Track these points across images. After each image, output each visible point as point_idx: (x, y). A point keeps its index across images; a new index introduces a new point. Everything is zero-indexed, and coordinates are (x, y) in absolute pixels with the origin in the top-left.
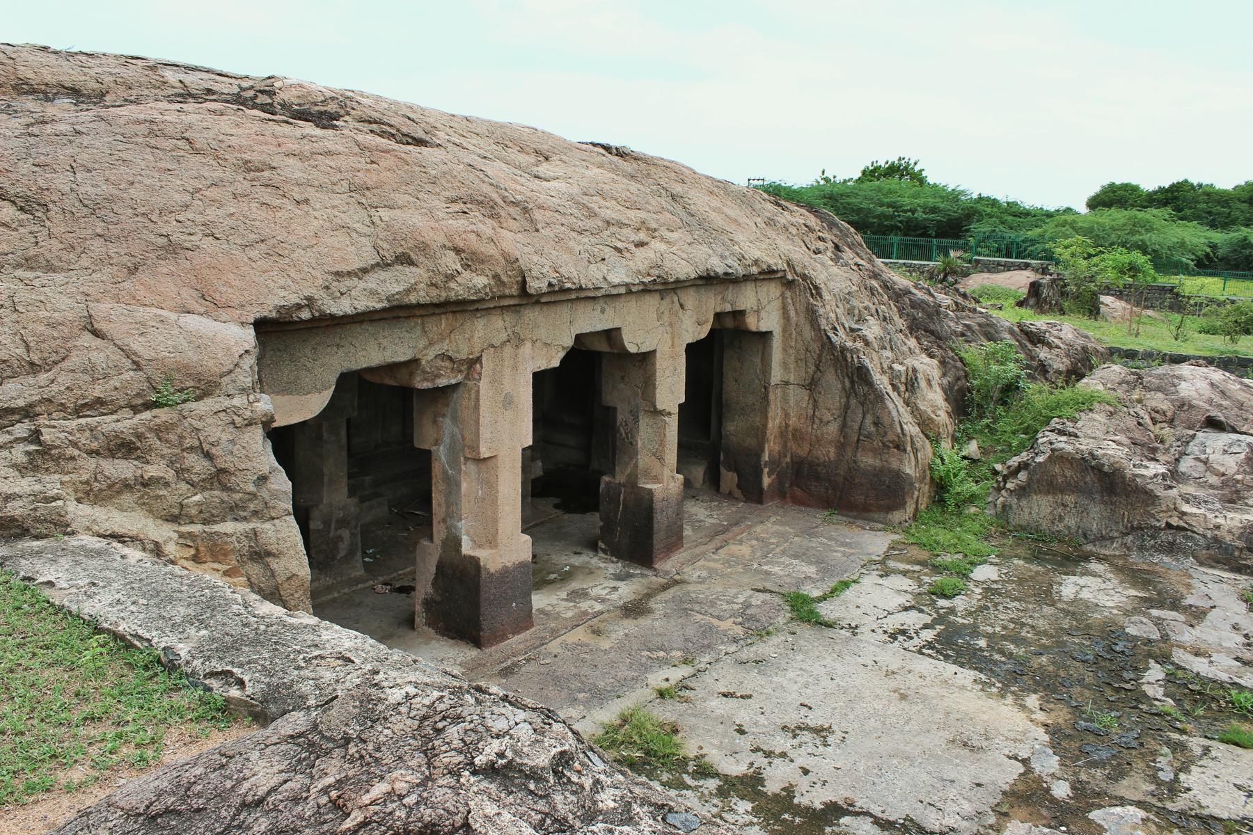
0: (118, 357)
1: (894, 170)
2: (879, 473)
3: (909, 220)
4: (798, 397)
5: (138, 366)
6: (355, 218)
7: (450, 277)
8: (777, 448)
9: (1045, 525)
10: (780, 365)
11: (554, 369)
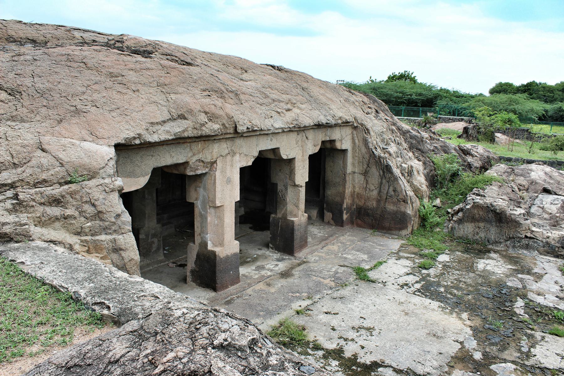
0: (53, 161)
1: (403, 77)
2: (396, 213)
3: (409, 99)
4: (359, 179)
5: (62, 165)
6: (160, 98)
7: (203, 125)
8: (350, 202)
9: (470, 236)
10: (351, 164)
11: (250, 166)
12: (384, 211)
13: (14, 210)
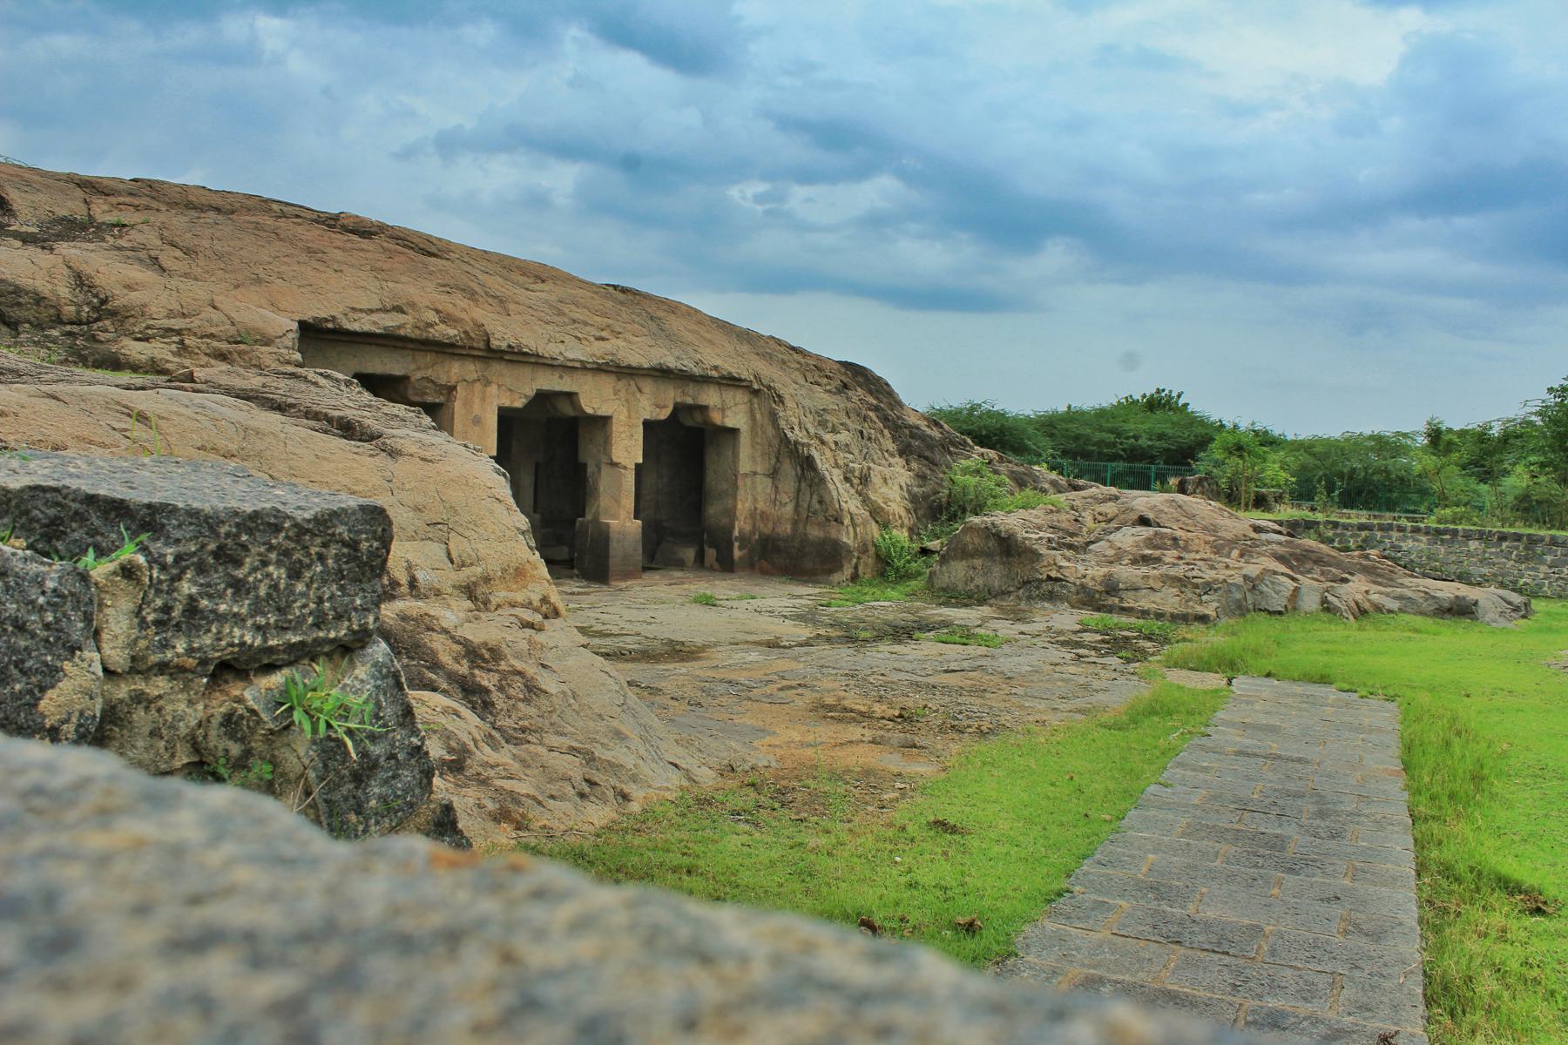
1: (1157, 404)
2: (824, 542)
3: (1133, 449)
4: (763, 485)
5: (233, 324)
7: (430, 325)
8: (748, 528)
10: (748, 458)
12: (805, 540)
13: (177, 354)
